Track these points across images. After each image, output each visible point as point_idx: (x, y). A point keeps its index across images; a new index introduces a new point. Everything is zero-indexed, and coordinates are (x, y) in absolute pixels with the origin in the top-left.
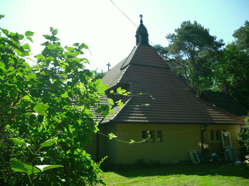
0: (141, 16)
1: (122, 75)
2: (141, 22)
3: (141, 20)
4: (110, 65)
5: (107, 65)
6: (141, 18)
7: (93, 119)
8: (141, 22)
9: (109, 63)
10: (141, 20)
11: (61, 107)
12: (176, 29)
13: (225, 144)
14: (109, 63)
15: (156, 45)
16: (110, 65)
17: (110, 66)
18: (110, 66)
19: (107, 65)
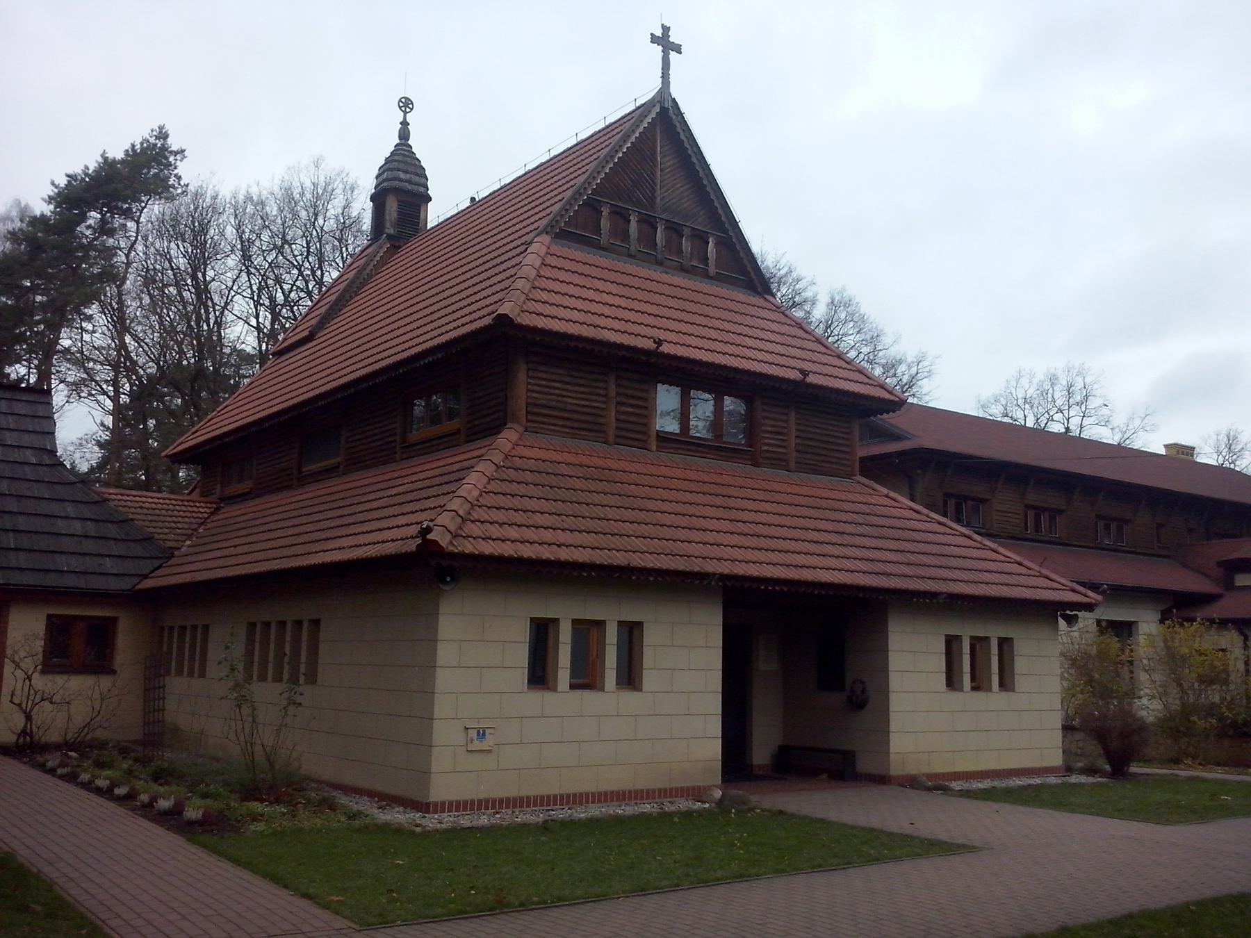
2: (404, 134)
3: (405, 124)
5: (654, 39)
8: (404, 134)
9: (666, 29)
10: (405, 124)
14: (666, 29)
16: (678, 49)
17: (673, 55)
18: (673, 55)
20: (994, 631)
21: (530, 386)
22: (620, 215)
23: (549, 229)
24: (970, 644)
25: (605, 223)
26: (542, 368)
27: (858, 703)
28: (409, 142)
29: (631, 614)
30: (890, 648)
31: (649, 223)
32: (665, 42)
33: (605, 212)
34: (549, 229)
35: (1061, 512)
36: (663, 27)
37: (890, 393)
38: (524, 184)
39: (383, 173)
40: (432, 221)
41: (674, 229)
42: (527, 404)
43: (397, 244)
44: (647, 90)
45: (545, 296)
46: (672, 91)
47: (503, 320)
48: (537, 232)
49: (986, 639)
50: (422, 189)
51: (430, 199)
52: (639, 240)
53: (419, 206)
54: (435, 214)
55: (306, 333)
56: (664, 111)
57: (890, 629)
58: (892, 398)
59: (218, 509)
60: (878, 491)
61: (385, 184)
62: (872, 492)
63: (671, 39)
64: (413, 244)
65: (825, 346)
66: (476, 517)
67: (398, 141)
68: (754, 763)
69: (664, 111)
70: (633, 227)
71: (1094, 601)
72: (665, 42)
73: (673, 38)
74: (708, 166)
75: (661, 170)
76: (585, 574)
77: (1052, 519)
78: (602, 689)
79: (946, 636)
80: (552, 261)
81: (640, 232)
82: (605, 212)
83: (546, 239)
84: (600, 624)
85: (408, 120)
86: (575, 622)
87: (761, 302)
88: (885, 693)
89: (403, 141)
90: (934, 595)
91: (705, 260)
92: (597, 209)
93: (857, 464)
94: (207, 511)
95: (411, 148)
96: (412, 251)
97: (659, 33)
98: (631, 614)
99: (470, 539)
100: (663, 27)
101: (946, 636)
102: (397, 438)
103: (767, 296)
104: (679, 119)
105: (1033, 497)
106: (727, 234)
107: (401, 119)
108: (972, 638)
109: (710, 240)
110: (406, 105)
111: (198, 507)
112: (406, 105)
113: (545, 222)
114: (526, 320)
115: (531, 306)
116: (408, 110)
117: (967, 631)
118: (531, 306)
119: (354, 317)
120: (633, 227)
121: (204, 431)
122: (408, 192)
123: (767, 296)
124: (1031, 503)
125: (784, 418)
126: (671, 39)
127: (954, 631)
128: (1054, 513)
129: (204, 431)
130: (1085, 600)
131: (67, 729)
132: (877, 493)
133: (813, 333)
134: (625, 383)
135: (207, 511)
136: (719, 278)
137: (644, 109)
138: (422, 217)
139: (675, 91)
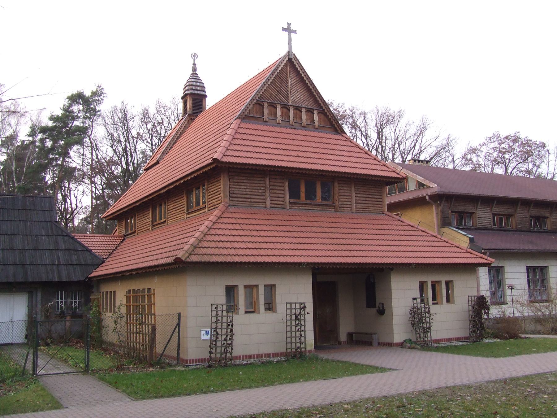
0: (194, 56)
1: (547, 313)
2: (194, 70)
3: (194, 64)
4: (295, 32)
5: (284, 29)
6: (194, 60)
7: (89, 248)
8: (194, 70)
9: (289, 25)
10: (194, 64)
11: (141, 333)
12: (526, 137)
13: (145, 297)
14: (289, 25)
15: (5, 160)
16: (295, 32)
17: (293, 35)
18: (293, 35)
19: (284, 29)
20: (443, 278)
21: (230, 186)
22: (273, 106)
23: (240, 117)
24: (432, 284)
25: (266, 111)
26: (236, 177)
27: (381, 312)
28: (197, 72)
29: (270, 281)
30: (392, 289)
31: (286, 107)
32: (289, 30)
33: (266, 105)
34: (240, 117)
35: (512, 215)
36: (288, 23)
37: (398, 174)
38: (254, 81)
39: (186, 87)
40: (208, 107)
41: (298, 109)
42: (230, 193)
43: (193, 118)
44: (280, 52)
45: (236, 147)
46: (293, 51)
47: (215, 160)
48: (235, 118)
49: (439, 282)
50: (203, 93)
51: (206, 96)
52: (282, 116)
53: (202, 100)
54: (209, 103)
55: (156, 161)
56: (290, 60)
57: (392, 280)
58: (398, 176)
59: (124, 239)
60: (395, 218)
61: (187, 92)
62: (392, 219)
63: (291, 29)
64: (200, 117)
65: (369, 155)
66: (201, 246)
67: (192, 72)
68: (341, 340)
69: (290, 60)
70: (279, 112)
71: (490, 262)
72: (289, 30)
73: (292, 28)
74: (311, 81)
75: (291, 85)
76: (246, 267)
77: (508, 219)
78: (259, 313)
79: (420, 282)
80: (240, 131)
81: (282, 112)
82: (266, 105)
83: (239, 121)
84: (257, 286)
85: (196, 63)
86: (246, 287)
87: (341, 137)
88: (391, 307)
89: (194, 72)
90: (410, 264)
91: (313, 121)
92: (262, 105)
93: (386, 207)
94: (119, 241)
95: (198, 75)
96: (200, 119)
97: (286, 27)
98: (270, 282)
99: (197, 255)
100: (288, 23)
101: (420, 282)
102: (222, 195)
103: (343, 134)
104: (297, 62)
105: (497, 210)
106: (323, 108)
107: (193, 63)
108: (432, 282)
109: (315, 112)
110: (194, 56)
111: (111, 242)
112: (194, 56)
113: (238, 113)
114: (226, 159)
115: (229, 153)
116: (195, 58)
117: (429, 279)
118: (229, 153)
119: (196, 139)
120: (279, 112)
121: (118, 206)
122: (198, 95)
123: (343, 134)
124: (496, 213)
125: (349, 189)
126: (287, 32)
127: (423, 279)
128: (509, 216)
129: (118, 206)
130: (485, 261)
131: (400, 370)
132: (394, 219)
133: (364, 149)
134: (274, 180)
135: (119, 241)
136: (320, 128)
137: (281, 60)
138: (203, 104)
139: (294, 51)
